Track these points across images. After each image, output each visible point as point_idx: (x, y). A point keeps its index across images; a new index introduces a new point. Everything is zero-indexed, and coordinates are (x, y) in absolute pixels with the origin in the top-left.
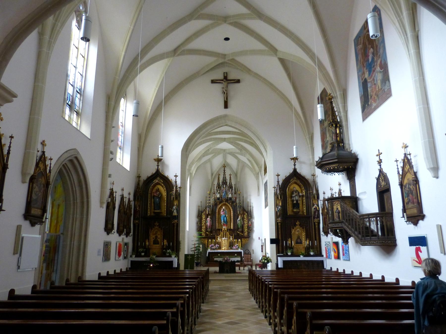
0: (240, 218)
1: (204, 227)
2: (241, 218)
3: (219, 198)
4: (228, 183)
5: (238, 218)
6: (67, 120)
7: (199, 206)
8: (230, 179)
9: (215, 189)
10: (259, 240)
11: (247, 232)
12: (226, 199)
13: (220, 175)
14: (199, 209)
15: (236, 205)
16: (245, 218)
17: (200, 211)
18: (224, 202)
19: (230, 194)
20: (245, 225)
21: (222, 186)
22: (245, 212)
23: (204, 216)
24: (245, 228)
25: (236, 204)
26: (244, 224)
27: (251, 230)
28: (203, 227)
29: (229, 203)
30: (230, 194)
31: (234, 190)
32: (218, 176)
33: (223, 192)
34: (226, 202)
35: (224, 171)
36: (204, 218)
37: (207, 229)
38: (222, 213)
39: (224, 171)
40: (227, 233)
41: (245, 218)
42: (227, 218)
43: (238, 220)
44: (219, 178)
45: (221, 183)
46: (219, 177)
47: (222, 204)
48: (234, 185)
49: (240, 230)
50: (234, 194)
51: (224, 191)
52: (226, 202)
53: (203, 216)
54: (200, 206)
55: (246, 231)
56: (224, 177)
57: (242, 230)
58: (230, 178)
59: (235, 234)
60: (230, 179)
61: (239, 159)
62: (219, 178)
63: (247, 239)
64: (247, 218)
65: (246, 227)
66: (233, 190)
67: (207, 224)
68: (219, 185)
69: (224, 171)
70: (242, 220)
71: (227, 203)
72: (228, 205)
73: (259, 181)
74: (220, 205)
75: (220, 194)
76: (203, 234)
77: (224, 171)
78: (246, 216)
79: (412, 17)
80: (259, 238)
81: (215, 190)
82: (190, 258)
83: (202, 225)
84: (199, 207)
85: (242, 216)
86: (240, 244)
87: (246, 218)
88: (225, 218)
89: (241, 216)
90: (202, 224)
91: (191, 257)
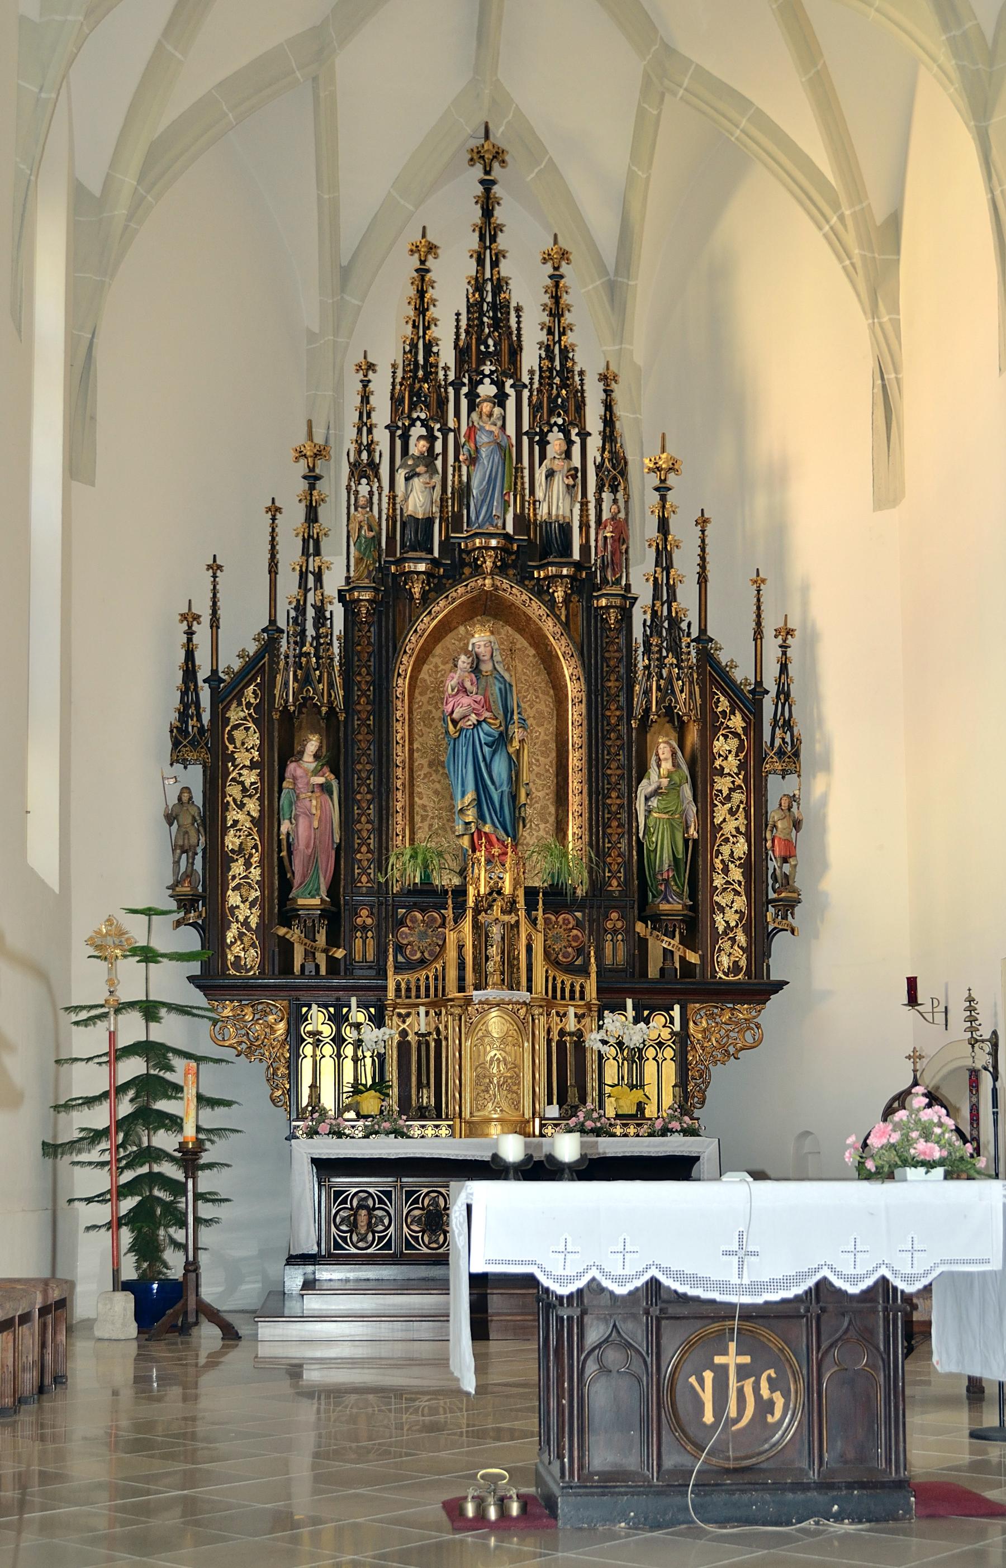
0: (667, 766)
1: (248, 865)
2: (675, 764)
3: (429, 521)
4: (530, 359)
5: (642, 772)
6: (50, 884)
7: (184, 617)
8: (556, 309)
9: (375, 418)
10: (911, 1013)
11: (747, 931)
12: (506, 536)
13: (432, 248)
14: (190, 655)
15: (626, 615)
16: (721, 772)
17: (203, 673)
18: (477, 570)
19: (559, 483)
20: (726, 850)
21: (457, 385)
22: (724, 704)
23: (254, 740)
24: (718, 881)
25: (628, 601)
26: (711, 830)
27: (788, 906)
28: (237, 868)
29: (541, 591)
30: (550, 474)
31: (594, 443)
32: (415, 262)
33: (473, 460)
34: (501, 569)
35: (487, 213)
36: (254, 765)
37: (286, 885)
38: (466, 700)
39: (488, 206)
40: (524, 928)
41: (721, 772)
42: (514, 765)
43: (645, 788)
44: (421, 293)
45: (447, 356)
46: (423, 272)
47: (460, 593)
48: (604, 378)
49: (673, 906)
50: (600, 489)
51: (483, 438)
52: (501, 569)
53: (239, 735)
54: (197, 618)
55: (732, 918)
56: (478, 286)
57: (694, 908)
58: (556, 298)
59: (608, 947)
60: (556, 309)
61: (668, 50)
62: (421, 293)
63: (743, 1012)
64: (742, 766)
65: (736, 874)
66: (584, 435)
67: (285, 827)
68: (430, 369)
69: (487, 213)
70: (687, 790)
71: (517, 595)
72: (536, 609)
73: (896, 324)
74: (442, 608)
75: (437, 479)
76: (237, 949)
77: (488, 206)
78: (733, 743)
79: (426, 1389)
80: (912, 983)
81: (382, 437)
82: (739, 1353)
83: (232, 841)
84: (190, 633)
85: (693, 735)
86: (670, 1070)
87: (731, 764)
88: (500, 767)
89: (681, 745)
90: (225, 830)
91: (732, 1346)
